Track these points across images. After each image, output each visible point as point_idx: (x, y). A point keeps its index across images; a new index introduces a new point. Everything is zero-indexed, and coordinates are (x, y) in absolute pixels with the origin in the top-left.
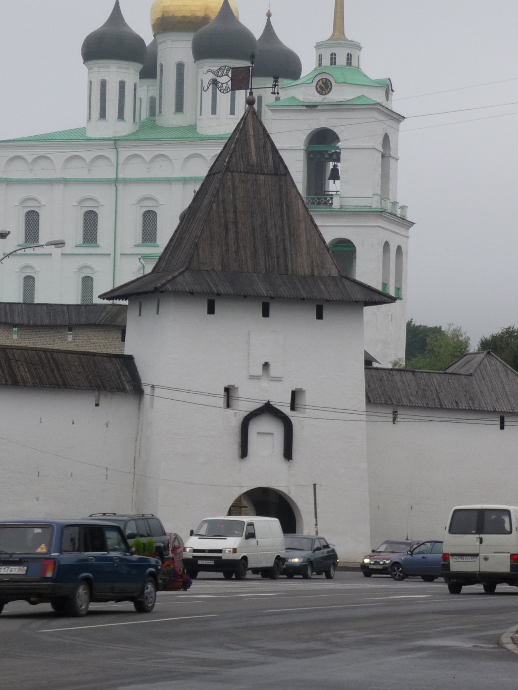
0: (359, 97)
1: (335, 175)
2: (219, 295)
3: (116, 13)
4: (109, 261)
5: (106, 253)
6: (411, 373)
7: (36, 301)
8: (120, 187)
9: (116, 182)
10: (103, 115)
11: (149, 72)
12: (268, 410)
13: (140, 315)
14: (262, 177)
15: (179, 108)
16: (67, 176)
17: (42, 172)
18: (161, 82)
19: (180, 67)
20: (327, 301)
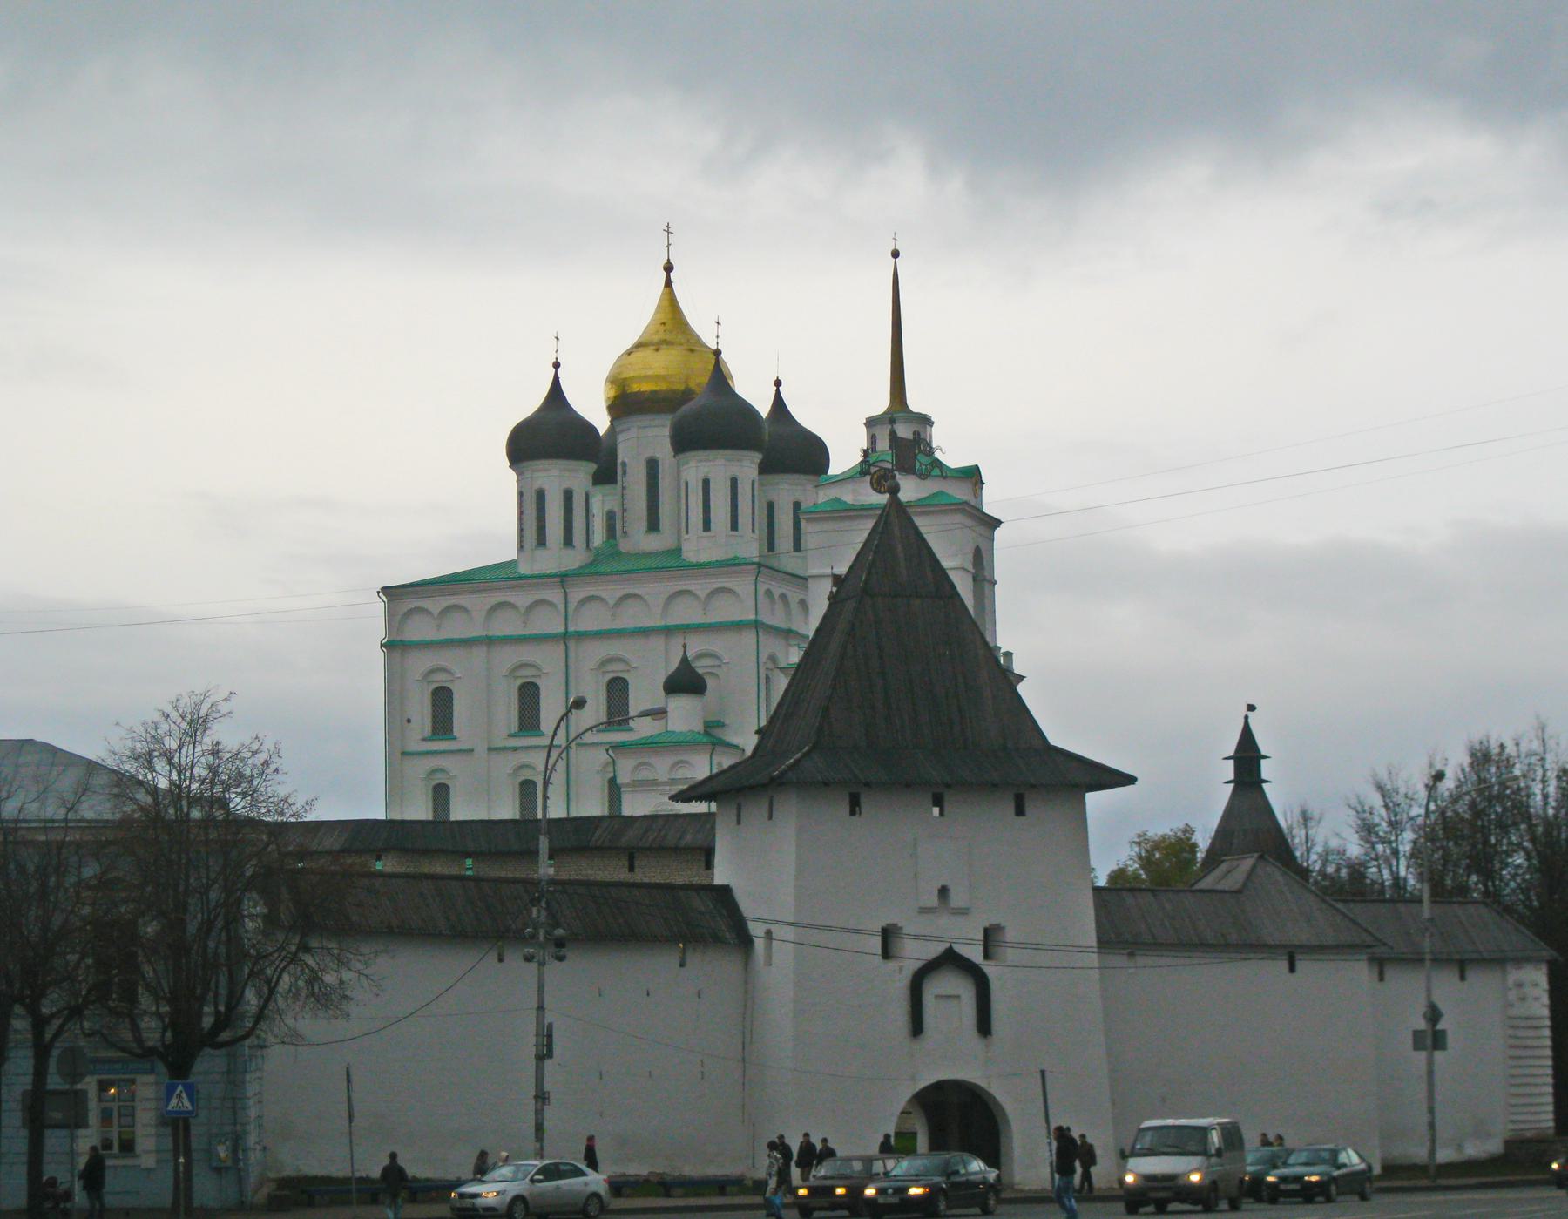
0: (934, 495)
2: (867, 785)
3: (556, 392)
6: (1149, 895)
7: (452, 818)
8: (572, 645)
9: (565, 637)
11: (606, 474)
12: (951, 960)
13: (739, 823)
14: (917, 602)
15: (653, 525)
19: (652, 465)
20: (1033, 786)
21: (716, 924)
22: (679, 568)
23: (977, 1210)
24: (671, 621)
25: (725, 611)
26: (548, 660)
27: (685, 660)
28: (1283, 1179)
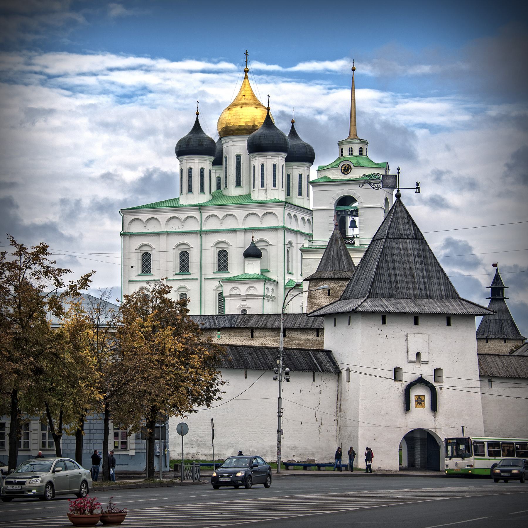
1: (353, 225)
3: (197, 127)
4: (197, 284)
5: (195, 278)
8: (203, 235)
10: (190, 190)
12: (421, 381)
13: (335, 326)
15: (238, 184)
16: (168, 230)
17: (152, 228)
18: (226, 167)
19: (238, 157)
21: (321, 364)
22: (250, 204)
23: (263, 486)
24: (247, 226)
25: (270, 222)
26: (193, 242)
27: (253, 243)
28: (502, 471)
